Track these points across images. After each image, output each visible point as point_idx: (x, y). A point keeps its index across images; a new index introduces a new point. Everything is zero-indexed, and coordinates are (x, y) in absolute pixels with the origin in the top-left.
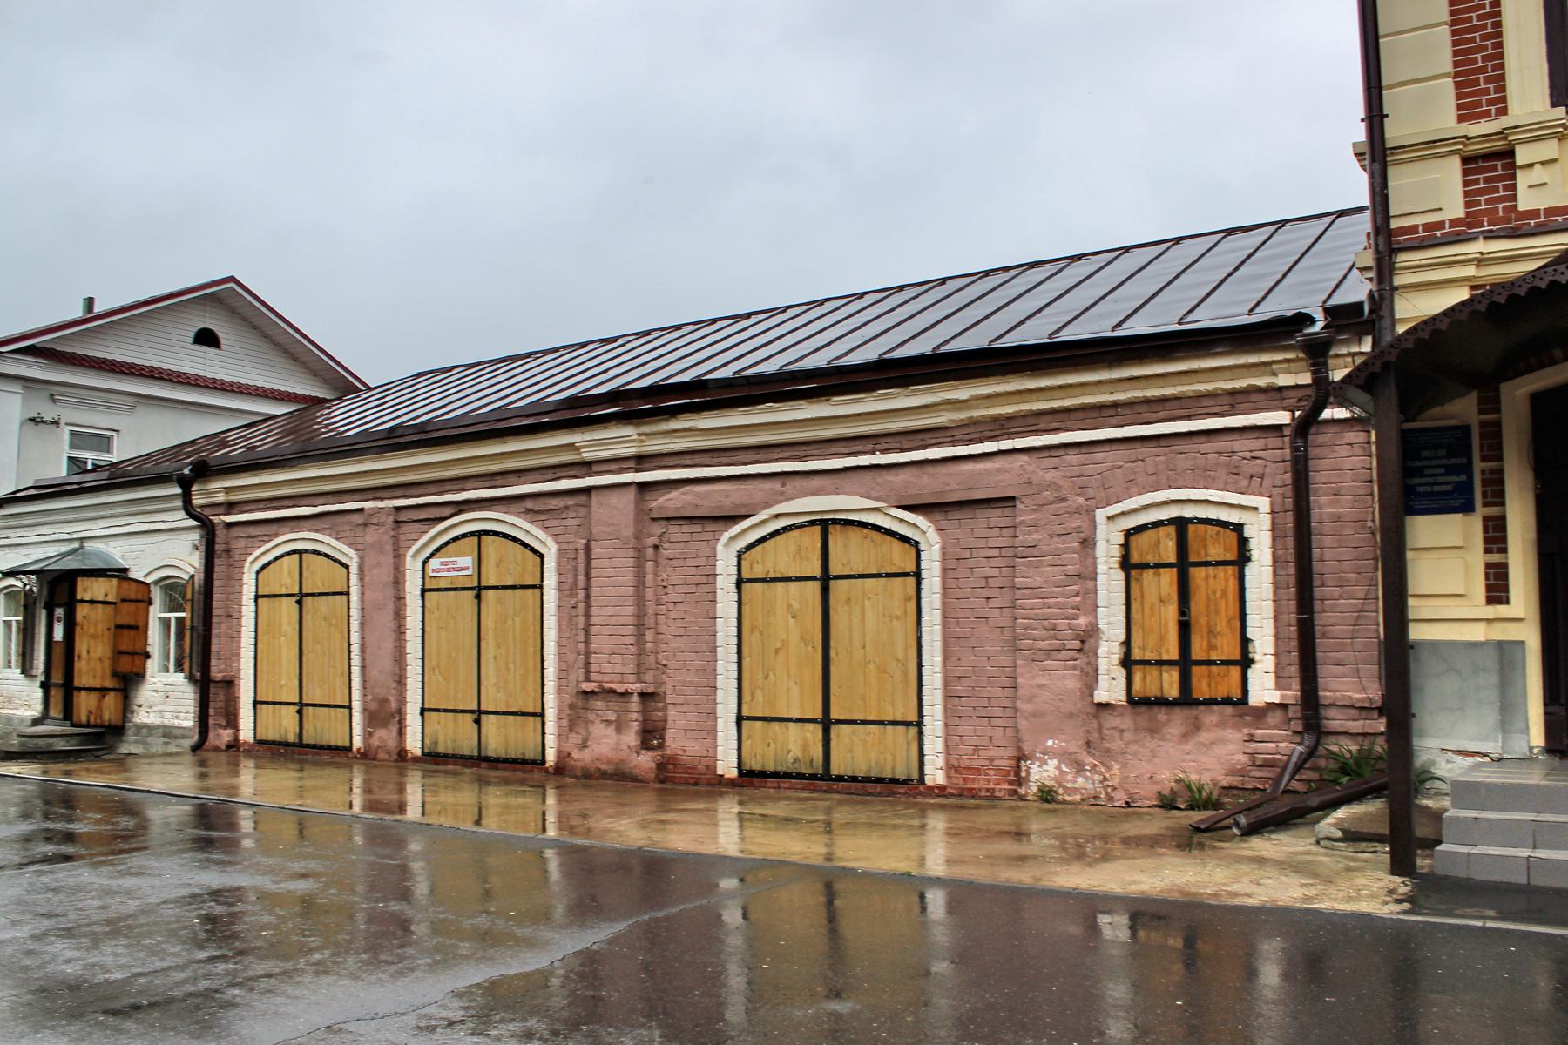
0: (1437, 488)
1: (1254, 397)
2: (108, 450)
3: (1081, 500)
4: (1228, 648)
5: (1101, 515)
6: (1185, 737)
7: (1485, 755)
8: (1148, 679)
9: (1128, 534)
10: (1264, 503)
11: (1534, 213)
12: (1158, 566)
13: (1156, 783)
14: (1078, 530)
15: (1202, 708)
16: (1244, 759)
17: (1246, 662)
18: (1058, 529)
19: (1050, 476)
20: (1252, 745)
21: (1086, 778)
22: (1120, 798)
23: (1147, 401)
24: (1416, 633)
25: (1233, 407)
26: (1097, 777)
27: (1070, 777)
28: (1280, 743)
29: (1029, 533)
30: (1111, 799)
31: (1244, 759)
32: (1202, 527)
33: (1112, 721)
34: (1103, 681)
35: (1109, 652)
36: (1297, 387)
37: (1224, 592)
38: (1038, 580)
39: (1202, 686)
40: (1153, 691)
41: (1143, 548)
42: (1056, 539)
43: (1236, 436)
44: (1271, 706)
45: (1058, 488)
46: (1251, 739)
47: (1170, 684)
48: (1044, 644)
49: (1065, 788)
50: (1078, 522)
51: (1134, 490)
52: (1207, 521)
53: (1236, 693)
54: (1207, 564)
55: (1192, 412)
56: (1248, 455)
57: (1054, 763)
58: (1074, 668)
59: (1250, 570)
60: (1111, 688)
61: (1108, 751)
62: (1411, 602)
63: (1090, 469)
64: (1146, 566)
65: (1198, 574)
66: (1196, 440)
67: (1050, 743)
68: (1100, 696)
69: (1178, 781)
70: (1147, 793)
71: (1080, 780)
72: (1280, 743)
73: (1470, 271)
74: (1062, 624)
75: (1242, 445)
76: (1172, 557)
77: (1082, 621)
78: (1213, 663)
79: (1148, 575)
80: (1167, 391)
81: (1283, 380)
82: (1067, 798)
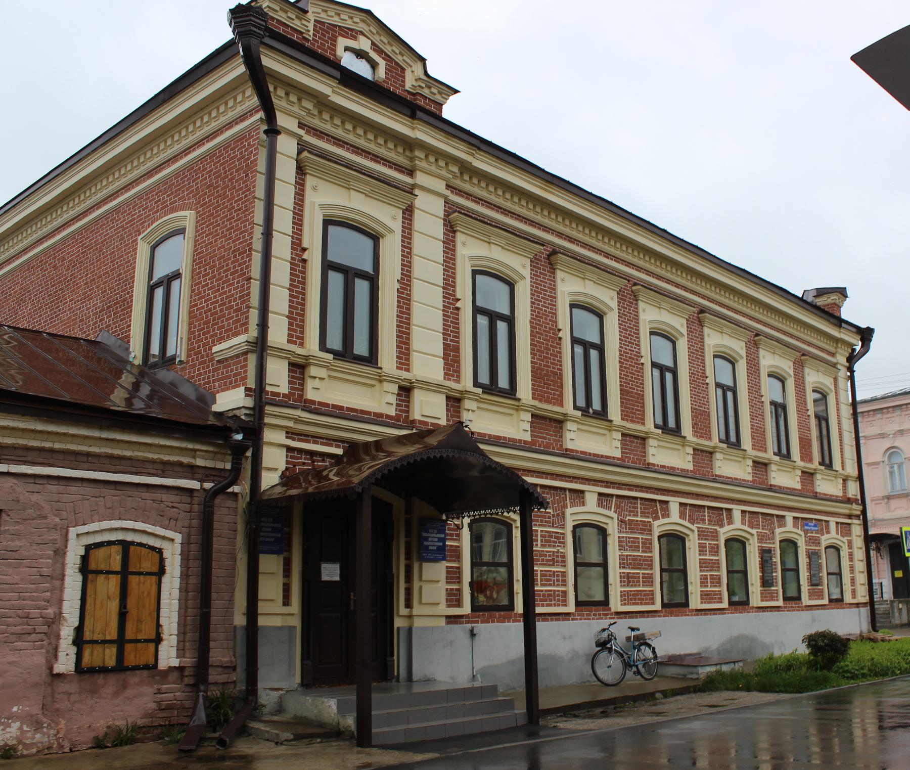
0: (267, 539)
1: (176, 469)
2: (295, 627)
3: (57, 520)
4: (148, 632)
5: (73, 532)
6: (116, 694)
7: (282, 689)
8: (95, 653)
9: (88, 548)
10: (178, 537)
11: (313, 402)
12: (109, 572)
13: (94, 730)
14: (54, 542)
15: (128, 673)
16: (154, 706)
17: (158, 640)
18: (38, 539)
19: (34, 498)
20: (159, 696)
21: (44, 734)
22: (67, 745)
23: (111, 457)
24: (262, 621)
25: (163, 471)
26: (52, 732)
27: (29, 735)
28: (174, 692)
29: (12, 540)
30: (62, 747)
31: (154, 706)
32: (139, 548)
33: (63, 687)
34: (61, 656)
35: (67, 633)
36: (205, 468)
37: (149, 594)
38: (16, 578)
39: (131, 659)
40: (97, 663)
41: (99, 559)
42: (35, 547)
43: (164, 491)
44: (172, 669)
45: (40, 508)
46: (159, 692)
47: (109, 656)
48: (18, 629)
49: (25, 745)
50: (56, 536)
51: (96, 517)
52: (141, 545)
53: (151, 661)
54: (140, 573)
55: (139, 470)
56: (171, 505)
57: (16, 725)
58: (42, 647)
59: (165, 580)
60: (65, 663)
61: (57, 710)
62: (260, 604)
63: (66, 498)
64: (100, 572)
65: (133, 580)
66: (140, 489)
67: (15, 709)
68: (59, 668)
69: (108, 727)
70: (87, 737)
71: (38, 736)
72: (174, 692)
73: (290, 424)
74: (35, 613)
75: (167, 497)
76: (117, 567)
77: (50, 611)
78: (138, 641)
79: (101, 579)
80: (128, 453)
81: (200, 462)
82: (25, 752)
